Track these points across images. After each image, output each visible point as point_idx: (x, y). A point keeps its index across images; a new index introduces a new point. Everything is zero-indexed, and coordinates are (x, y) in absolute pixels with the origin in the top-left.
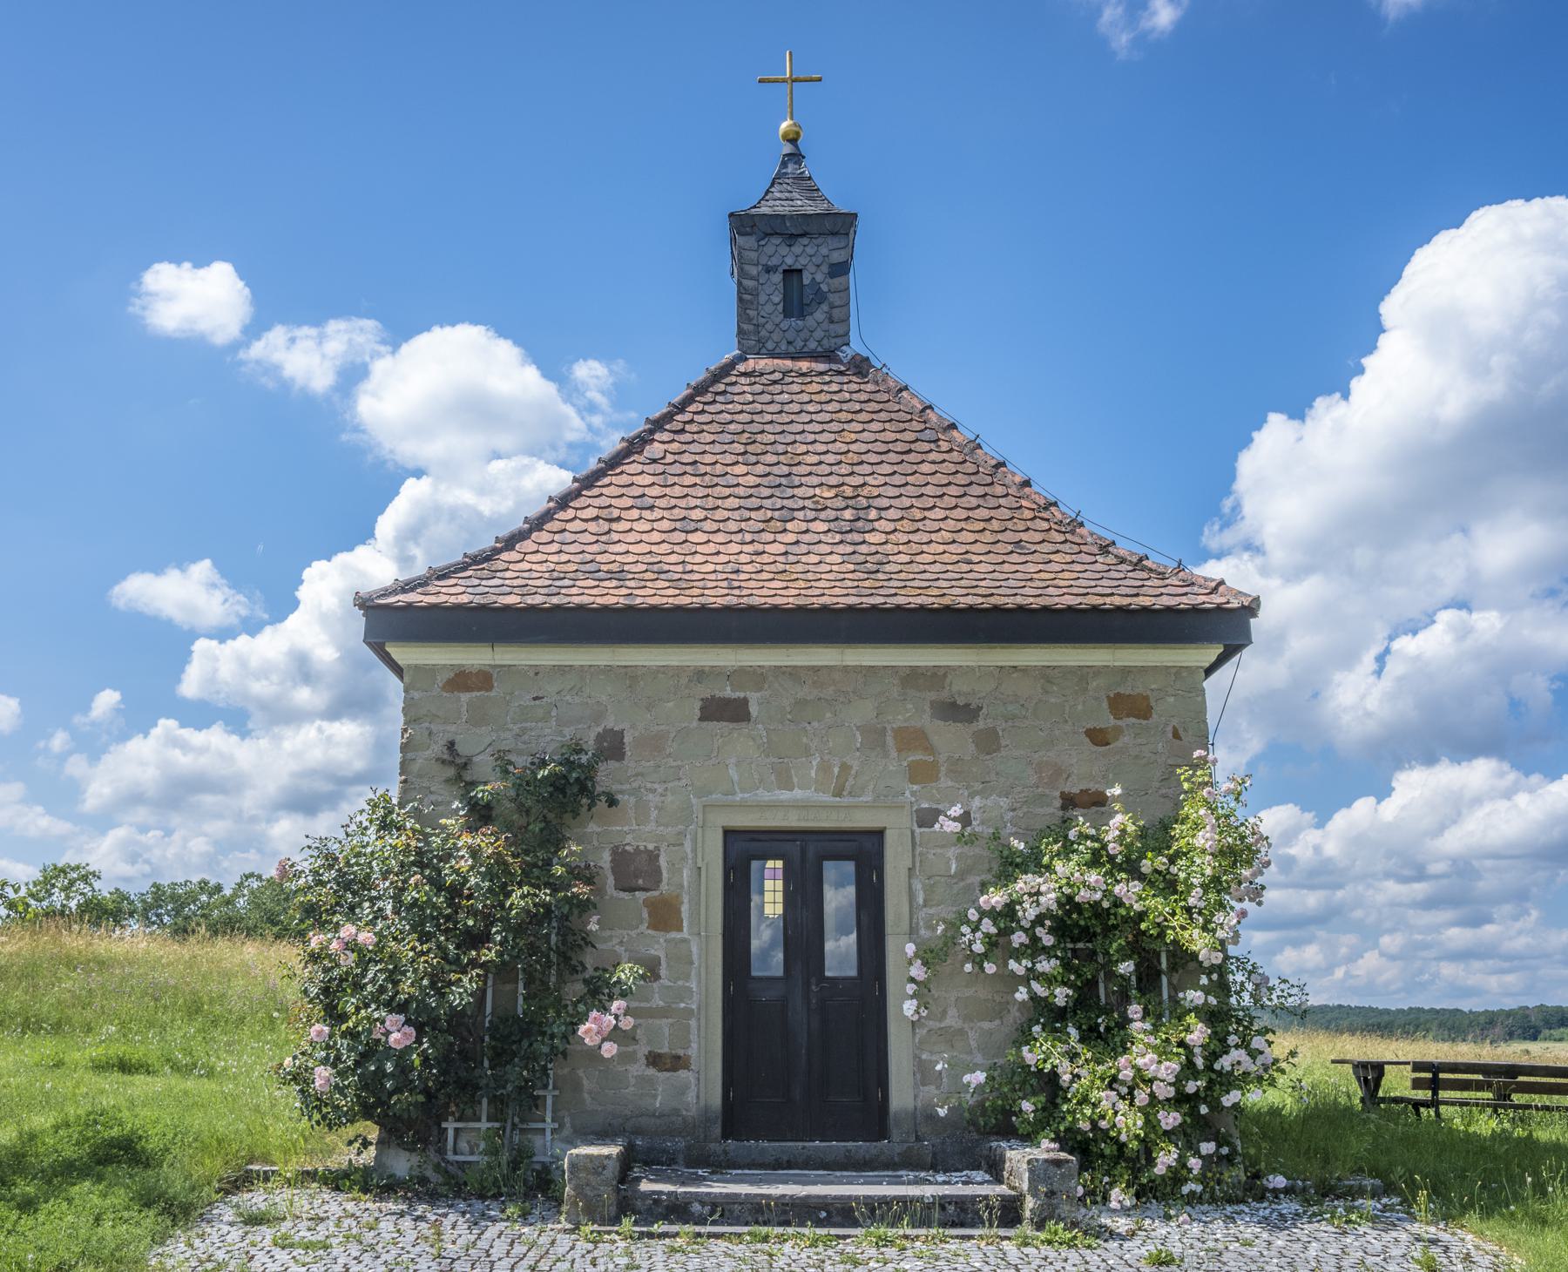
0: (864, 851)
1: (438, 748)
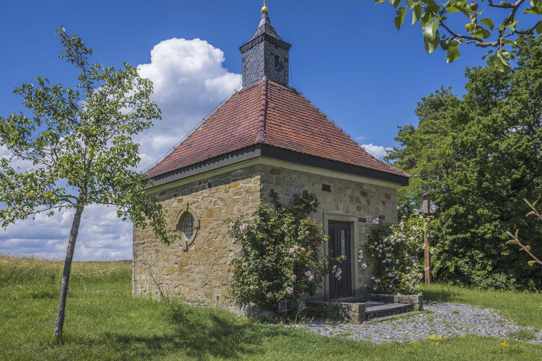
1: (269, 191)
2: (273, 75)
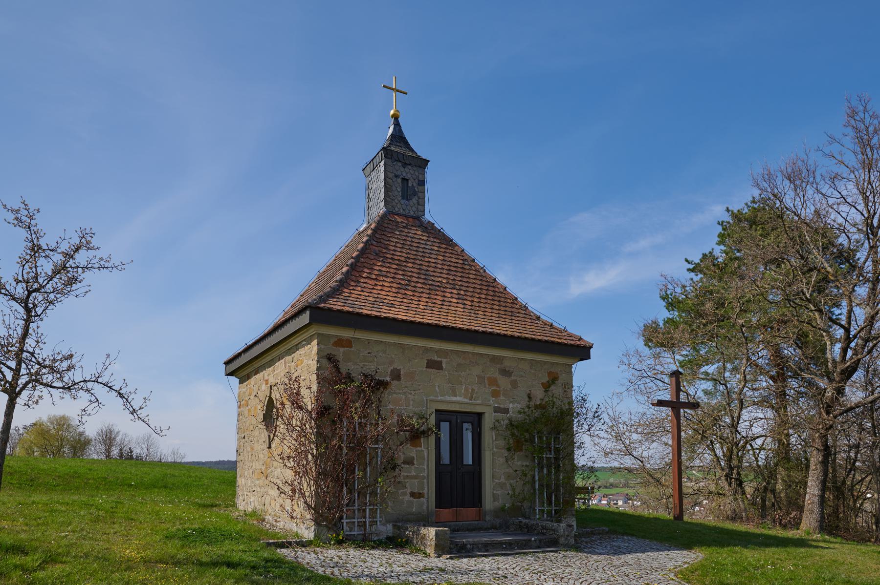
0: (477, 419)
2: (399, 206)
